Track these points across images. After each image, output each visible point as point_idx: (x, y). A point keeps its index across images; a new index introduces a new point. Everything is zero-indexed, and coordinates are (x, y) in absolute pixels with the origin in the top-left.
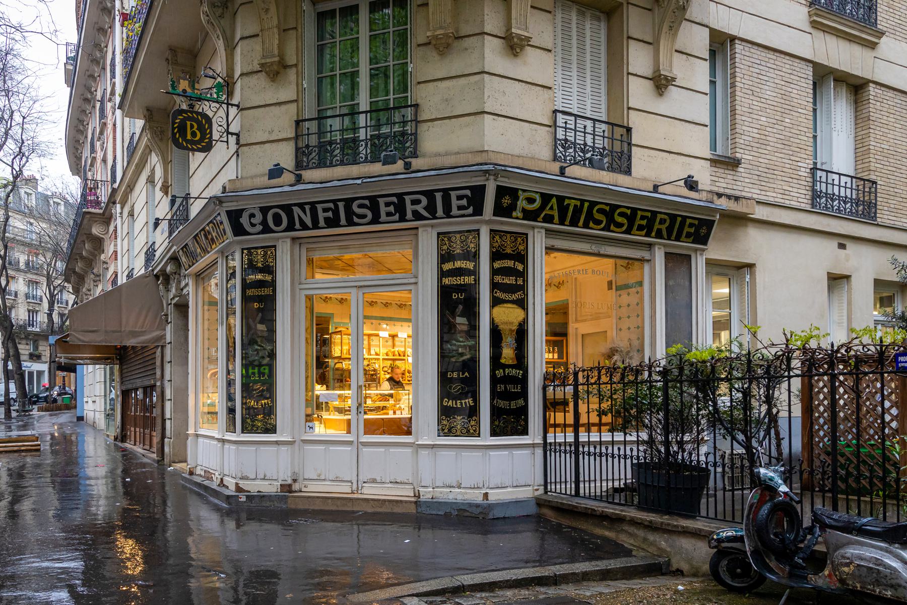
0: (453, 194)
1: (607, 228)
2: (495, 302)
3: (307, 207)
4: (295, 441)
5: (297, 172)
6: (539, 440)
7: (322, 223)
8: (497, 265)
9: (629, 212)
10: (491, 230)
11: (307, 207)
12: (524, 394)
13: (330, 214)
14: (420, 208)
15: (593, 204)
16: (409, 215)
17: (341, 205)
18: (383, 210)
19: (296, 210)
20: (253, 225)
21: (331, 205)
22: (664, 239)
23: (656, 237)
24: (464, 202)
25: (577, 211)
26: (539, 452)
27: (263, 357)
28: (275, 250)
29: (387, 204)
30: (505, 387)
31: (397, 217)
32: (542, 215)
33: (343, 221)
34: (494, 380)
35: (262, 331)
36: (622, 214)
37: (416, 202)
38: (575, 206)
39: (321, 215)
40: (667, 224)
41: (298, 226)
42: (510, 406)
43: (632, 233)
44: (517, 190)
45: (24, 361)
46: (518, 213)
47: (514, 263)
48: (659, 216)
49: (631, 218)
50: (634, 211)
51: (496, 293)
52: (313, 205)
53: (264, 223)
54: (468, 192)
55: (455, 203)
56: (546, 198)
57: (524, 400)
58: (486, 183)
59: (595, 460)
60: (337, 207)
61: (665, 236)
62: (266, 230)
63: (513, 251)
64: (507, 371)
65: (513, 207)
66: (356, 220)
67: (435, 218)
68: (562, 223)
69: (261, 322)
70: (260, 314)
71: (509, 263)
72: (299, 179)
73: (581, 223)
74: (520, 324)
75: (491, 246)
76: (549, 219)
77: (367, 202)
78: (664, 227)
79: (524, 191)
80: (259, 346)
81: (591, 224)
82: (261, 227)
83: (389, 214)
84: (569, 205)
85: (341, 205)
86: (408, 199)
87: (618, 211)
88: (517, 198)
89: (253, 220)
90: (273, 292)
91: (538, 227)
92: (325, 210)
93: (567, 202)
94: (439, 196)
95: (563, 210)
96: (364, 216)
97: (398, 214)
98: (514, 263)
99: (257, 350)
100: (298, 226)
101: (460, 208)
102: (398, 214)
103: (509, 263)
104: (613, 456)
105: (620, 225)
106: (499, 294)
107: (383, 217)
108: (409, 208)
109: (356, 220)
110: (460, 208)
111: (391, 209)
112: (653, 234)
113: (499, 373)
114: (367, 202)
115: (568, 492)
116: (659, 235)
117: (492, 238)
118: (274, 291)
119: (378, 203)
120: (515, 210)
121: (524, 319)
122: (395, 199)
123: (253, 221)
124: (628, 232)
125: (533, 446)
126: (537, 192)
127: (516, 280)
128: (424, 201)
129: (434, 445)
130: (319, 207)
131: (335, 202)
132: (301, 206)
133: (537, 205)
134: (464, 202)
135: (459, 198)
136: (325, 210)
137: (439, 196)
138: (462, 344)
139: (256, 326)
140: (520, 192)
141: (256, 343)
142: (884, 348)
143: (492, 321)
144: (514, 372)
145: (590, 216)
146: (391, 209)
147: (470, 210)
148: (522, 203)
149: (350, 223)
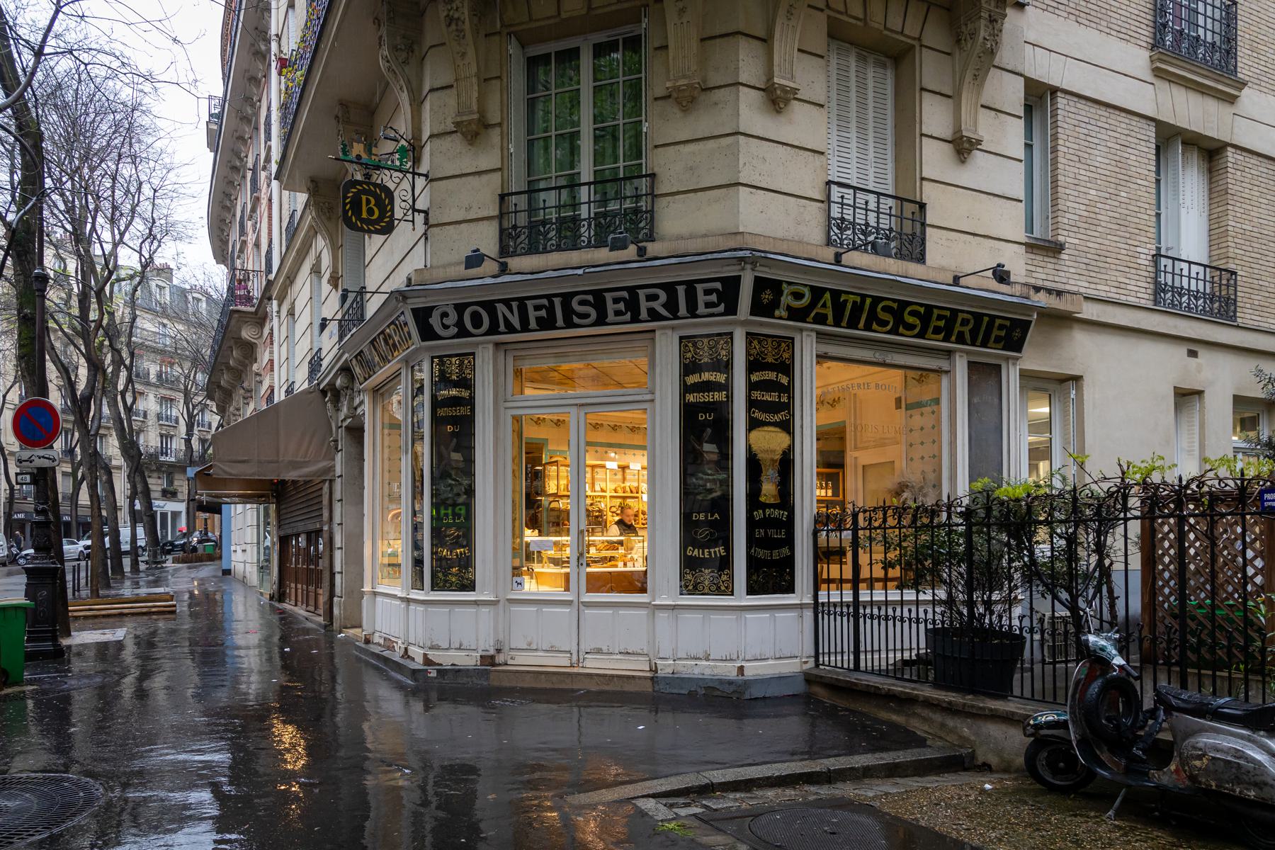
0: (700, 288)
1: (894, 331)
2: (753, 424)
3: (514, 304)
4: (499, 601)
6: (808, 600)
7: (533, 324)
8: (755, 377)
9: (922, 310)
11: (514, 304)
12: (790, 541)
13: (543, 313)
14: (657, 305)
15: (876, 300)
16: (644, 314)
17: (557, 301)
19: (501, 308)
20: (446, 327)
21: (545, 302)
23: (957, 342)
24: (714, 298)
25: (857, 309)
28: (474, 359)
30: (766, 533)
31: (628, 316)
32: (812, 315)
33: (560, 322)
34: (751, 524)
35: (457, 461)
36: (912, 313)
38: (855, 303)
39: (532, 315)
40: (971, 326)
41: (502, 328)
42: (771, 556)
44: (780, 282)
48: (961, 316)
50: (929, 308)
52: (522, 301)
53: (460, 324)
54: (718, 285)
55: (701, 299)
56: (817, 292)
59: (848, 621)
60: (552, 303)
65: (775, 304)
66: (576, 320)
67: (677, 318)
68: (837, 324)
71: (771, 375)
72: (504, 269)
73: (861, 325)
75: (748, 354)
77: (590, 298)
79: (790, 283)
81: (875, 326)
84: (846, 301)
85: (557, 301)
86: (642, 294)
88: (780, 293)
89: (446, 321)
92: (537, 308)
94: (681, 290)
95: (839, 308)
96: (587, 316)
97: (629, 313)
99: (450, 485)
100: (502, 328)
102: (629, 313)
103: (771, 375)
106: (758, 415)
107: (611, 317)
108: (644, 305)
109: (576, 320)
110: (708, 305)
111: (621, 306)
112: (953, 338)
113: (758, 514)
114: (590, 298)
115: (846, 666)
116: (960, 340)
118: (473, 410)
122: (625, 294)
124: (921, 335)
125: (801, 606)
126: (806, 285)
127: (779, 397)
128: (663, 296)
131: (549, 297)
132: (507, 303)
133: (806, 300)
136: (537, 308)
137: (681, 290)
140: (784, 285)
144: (776, 513)
145: (872, 316)
147: (721, 308)
148: (786, 299)
149: (569, 324)
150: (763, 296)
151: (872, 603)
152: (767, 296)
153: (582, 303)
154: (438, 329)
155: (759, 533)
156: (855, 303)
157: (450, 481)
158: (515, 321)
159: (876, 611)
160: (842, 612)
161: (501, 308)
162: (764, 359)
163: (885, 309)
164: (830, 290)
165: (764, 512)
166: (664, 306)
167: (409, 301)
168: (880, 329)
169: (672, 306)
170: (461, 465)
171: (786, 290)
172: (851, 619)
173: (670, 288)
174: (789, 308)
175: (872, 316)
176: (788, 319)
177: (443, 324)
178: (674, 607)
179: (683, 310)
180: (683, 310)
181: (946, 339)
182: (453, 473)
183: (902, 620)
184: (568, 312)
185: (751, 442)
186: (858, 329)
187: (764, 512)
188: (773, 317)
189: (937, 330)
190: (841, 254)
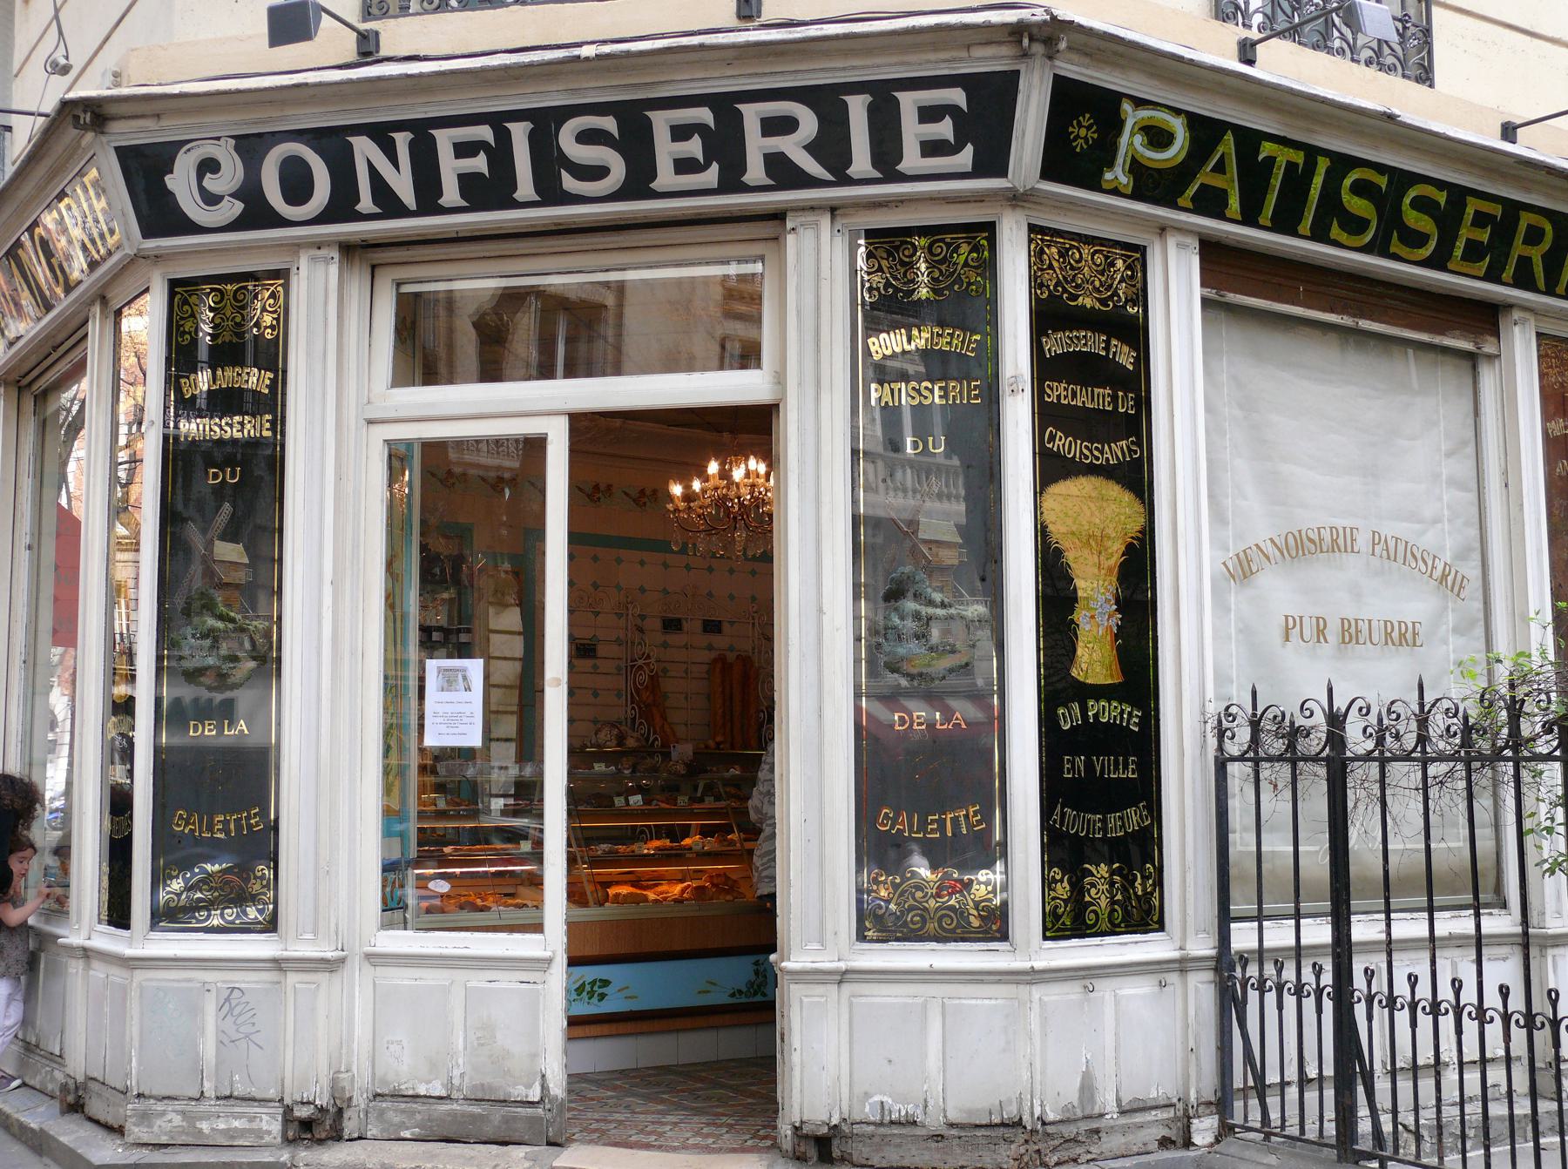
0: (908, 102)
1: (1379, 247)
2: (1050, 469)
3: (402, 140)
4: (342, 960)
5: (363, 26)
6: (1204, 947)
7: (451, 194)
8: (1056, 344)
9: (1442, 198)
10: (1032, 228)
11: (402, 140)
12: (1147, 791)
13: (479, 163)
14: (793, 147)
15: (1343, 163)
16: (755, 171)
17: (519, 133)
18: (666, 151)
19: (364, 148)
20: (211, 199)
21: (485, 133)
22: (1536, 290)
23: (1517, 284)
24: (944, 129)
25: (1297, 181)
26: (1201, 990)
27: (234, 659)
28: (286, 287)
29: (680, 133)
30: (1089, 766)
31: (711, 176)
32: (1192, 191)
33: (525, 188)
34: (1053, 742)
35: (235, 565)
36: (1421, 204)
37: (778, 126)
38: (1291, 166)
39: (450, 168)
40: (1546, 245)
41: (366, 204)
42: (1104, 829)
43: (1450, 266)
44: (1117, 97)
45: (1093, 1109)
46: (1118, 174)
47: (1108, 342)
48: (1526, 219)
49: (1448, 221)
50: (1459, 194)
51: (1052, 438)
52: (422, 131)
53: (250, 193)
54: (957, 97)
55: (913, 132)
56: (1205, 131)
57: (1149, 808)
58: (1022, 68)
59: (1280, 1007)
60: (504, 137)
61: (1541, 284)
62: (257, 214)
63: (1103, 302)
64: (1093, 707)
65: (1105, 152)
66: (569, 183)
67: (844, 180)
68: (1249, 219)
69: (230, 535)
70: (227, 508)
71: (1091, 343)
72: (368, 48)
73: (1306, 226)
74: (1130, 548)
75: (1035, 282)
76: (1211, 203)
77: (609, 124)
78: (1536, 254)
79: (1139, 103)
80: (221, 617)
81: (1336, 232)
82: (239, 207)
83: (684, 166)
84: (1271, 160)
85: (519, 133)
86: (751, 114)
87: (1413, 193)
88: (1119, 125)
89: (210, 183)
90: (273, 429)
91: (1182, 230)
92: (464, 150)
93: (1267, 149)
94: (857, 107)
95: (1254, 175)
96: (600, 172)
97: (715, 167)
98: (1108, 342)
99: (210, 634)
100: (366, 204)
101: (932, 148)
102: (715, 167)
103: (1091, 343)
104: (1299, 991)
105: (1418, 239)
106: (1061, 443)
107: (666, 177)
108: (756, 146)
109: (569, 183)
110: (932, 148)
111: (694, 147)
112: (1508, 274)
113: (1069, 718)
114: (609, 124)
115: (1312, 1134)
116: (1524, 280)
117: (1037, 258)
118: (279, 424)
119: (647, 128)
120: (1111, 164)
121: (1142, 532)
122: (705, 115)
123: (212, 183)
124: (1438, 261)
125: (1183, 965)
126: (1177, 112)
127: (1114, 398)
128: (809, 123)
129: (847, 972)
130: (444, 139)
131: (499, 121)
132: (381, 134)
133: (1177, 150)
134: (944, 129)
135: (929, 114)
136: (464, 150)
137: (857, 107)
138: (940, 612)
139: (209, 545)
140: (1127, 106)
141: (209, 607)
142: (1419, 749)
143: (1042, 532)
144: (1107, 711)
145: (1331, 204)
146: (694, 147)
147: (965, 159)
148: (1131, 142)
149: (550, 193)
150: (1073, 130)
151: (1261, 953)
152: (1083, 132)
153: (586, 137)
154: (192, 208)
155: (1074, 766)
156: (1291, 166)
157: (211, 622)
158: (403, 185)
159: (1270, 970)
160: (1262, 982)
161: (364, 148)
162: (1075, 298)
163: (1360, 188)
164: (1238, 130)
165: (1084, 710)
166: (812, 148)
167: (115, 127)
168: (1343, 237)
169: (831, 148)
170: (241, 577)
171: (1132, 117)
172: (1328, 1005)
173: (827, 101)
174: (1137, 168)
175: (1331, 204)
176: (1136, 195)
177: (202, 189)
178: (843, 977)
179: (861, 163)
180: (861, 163)
181: (1493, 276)
182: (218, 596)
183: (1299, 991)
184: (548, 160)
185: (1049, 517)
186: (1295, 234)
187: (1084, 710)
188: (1095, 186)
189: (1474, 252)
190: (1254, 44)
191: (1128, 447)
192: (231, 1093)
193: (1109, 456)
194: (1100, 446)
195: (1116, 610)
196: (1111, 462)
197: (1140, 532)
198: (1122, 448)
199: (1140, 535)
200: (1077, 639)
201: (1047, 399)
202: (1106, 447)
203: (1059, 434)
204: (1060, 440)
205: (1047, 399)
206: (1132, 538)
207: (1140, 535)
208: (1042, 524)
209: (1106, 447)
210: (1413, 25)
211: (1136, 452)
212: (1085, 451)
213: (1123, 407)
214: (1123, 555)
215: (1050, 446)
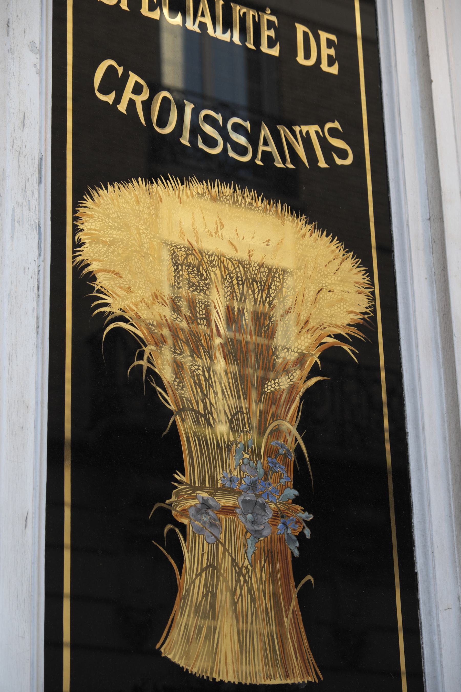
191: (323, 141)
192: (288, 280)
193: (272, 148)
194: (339, 162)
195: (296, 501)
196: (279, 164)
197: (358, 326)
198: (307, 141)
199: (359, 335)
200: (180, 561)
201: (336, 125)
202: (265, 131)
203: (133, 78)
204: (137, 90)
205: (336, 125)
206: (338, 336)
207: (359, 335)
208: (77, 270)
209: (265, 131)
210: (287, 527)
211: (343, 154)
212: (208, 129)
213: (307, 56)
214: (314, 371)
215: (110, 98)
